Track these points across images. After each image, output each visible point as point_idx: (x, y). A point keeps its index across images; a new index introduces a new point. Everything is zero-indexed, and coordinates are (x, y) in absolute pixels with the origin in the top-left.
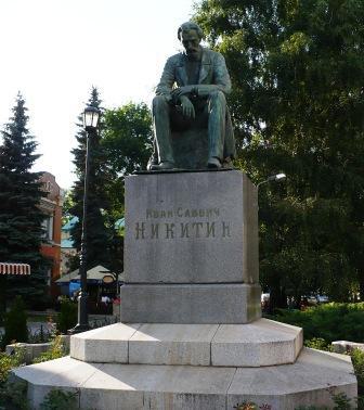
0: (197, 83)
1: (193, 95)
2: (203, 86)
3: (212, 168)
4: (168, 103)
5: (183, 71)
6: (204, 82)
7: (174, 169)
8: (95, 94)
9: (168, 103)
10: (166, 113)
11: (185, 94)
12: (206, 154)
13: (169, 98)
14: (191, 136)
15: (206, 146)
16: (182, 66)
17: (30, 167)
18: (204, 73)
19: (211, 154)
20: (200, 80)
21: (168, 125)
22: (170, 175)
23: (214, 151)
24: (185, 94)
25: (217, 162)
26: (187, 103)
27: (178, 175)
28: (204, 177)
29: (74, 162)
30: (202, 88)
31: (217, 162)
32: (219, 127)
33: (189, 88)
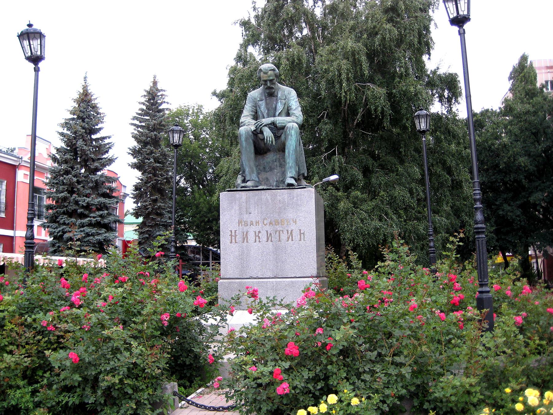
0: (274, 116)
1: (273, 127)
3: (290, 186)
4: (252, 132)
6: (280, 115)
9: (252, 132)
13: (253, 128)
14: (270, 157)
20: (277, 113)
24: (265, 125)
26: (268, 133)
28: (283, 194)
30: (280, 120)
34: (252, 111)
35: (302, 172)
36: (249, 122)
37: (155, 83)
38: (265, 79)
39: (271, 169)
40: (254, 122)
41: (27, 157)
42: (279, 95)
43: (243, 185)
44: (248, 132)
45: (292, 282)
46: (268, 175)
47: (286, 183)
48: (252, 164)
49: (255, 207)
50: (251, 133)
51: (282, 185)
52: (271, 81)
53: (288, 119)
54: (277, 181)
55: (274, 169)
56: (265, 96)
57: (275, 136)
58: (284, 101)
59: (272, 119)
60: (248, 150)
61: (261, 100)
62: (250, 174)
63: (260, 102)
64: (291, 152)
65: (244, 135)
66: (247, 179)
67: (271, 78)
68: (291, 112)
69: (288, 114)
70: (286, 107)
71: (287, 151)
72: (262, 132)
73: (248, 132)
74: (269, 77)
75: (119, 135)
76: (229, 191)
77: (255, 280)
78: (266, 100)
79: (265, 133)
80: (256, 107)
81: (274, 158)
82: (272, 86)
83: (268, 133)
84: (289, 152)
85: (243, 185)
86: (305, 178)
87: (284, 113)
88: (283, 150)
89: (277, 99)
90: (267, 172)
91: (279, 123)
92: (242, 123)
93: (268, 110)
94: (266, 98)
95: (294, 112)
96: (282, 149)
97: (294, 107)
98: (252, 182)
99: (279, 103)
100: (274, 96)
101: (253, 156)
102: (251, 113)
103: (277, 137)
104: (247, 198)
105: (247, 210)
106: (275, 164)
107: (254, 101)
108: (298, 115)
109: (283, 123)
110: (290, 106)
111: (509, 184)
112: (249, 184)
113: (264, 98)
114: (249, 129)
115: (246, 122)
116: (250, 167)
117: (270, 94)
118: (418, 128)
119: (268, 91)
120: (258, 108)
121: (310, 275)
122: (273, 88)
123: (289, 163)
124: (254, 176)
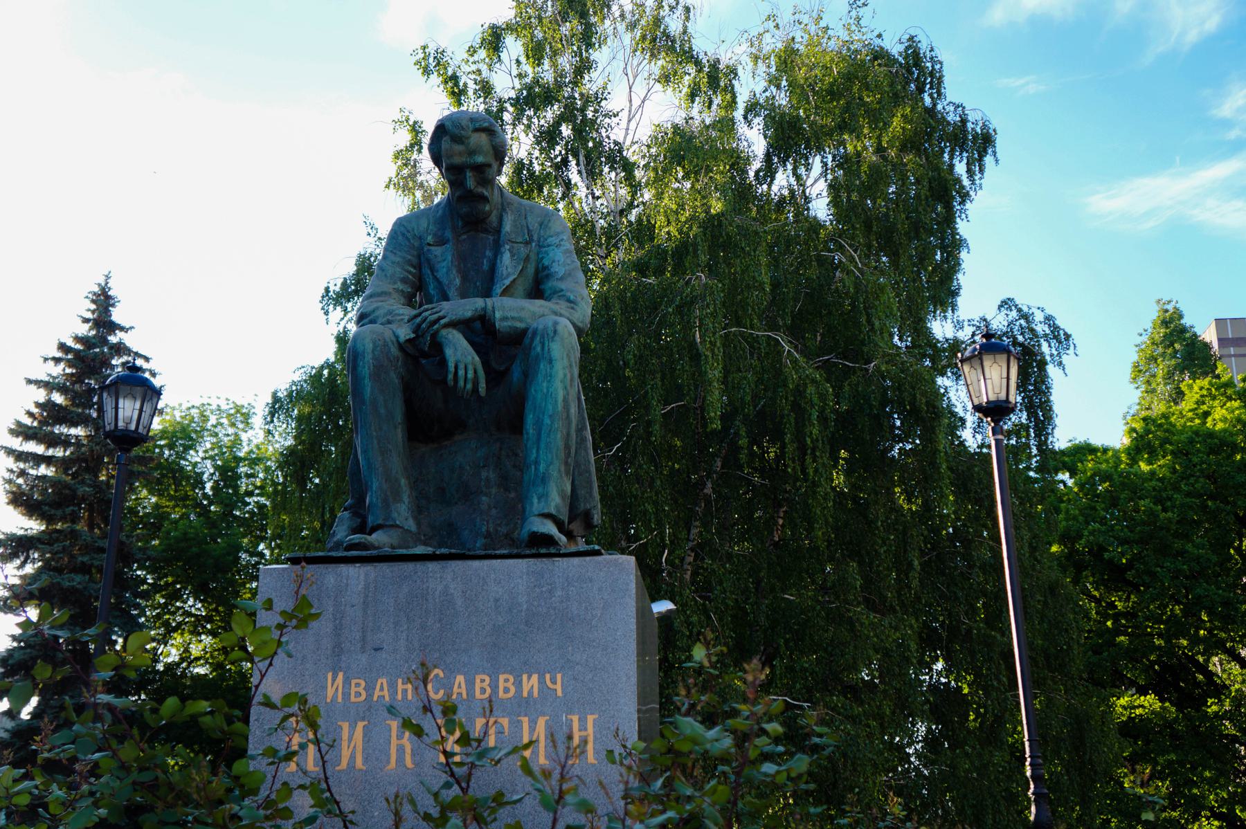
0: (487, 294)
1: (481, 331)
2: (508, 302)
3: (540, 546)
4: (401, 347)
5: (444, 259)
6: (506, 292)
7: (420, 550)
8: (104, 300)
9: (401, 347)
10: (394, 377)
11: (453, 324)
12: (515, 509)
13: (405, 333)
14: (467, 453)
15: (515, 483)
16: (441, 242)
17: (944, 293)
18: (508, 265)
19: (536, 506)
20: (498, 289)
21: (399, 416)
22: (409, 567)
23: (543, 497)
24: (453, 324)
25: (551, 528)
26: (460, 351)
27: (432, 566)
28: (511, 577)
29: (274, 395)
30: (510, 310)
31: (551, 528)
32: (558, 424)
33: (468, 307)
35: (582, 507)
36: (390, 312)
38: (457, 160)
40: (408, 312)
41: (322, 776)
42: (507, 227)
43: (357, 538)
44: (385, 345)
47: (525, 533)
48: (396, 463)
49: (396, 624)
50: (394, 351)
53: (537, 305)
58: (523, 251)
59: (479, 303)
60: (382, 411)
63: (437, 251)
65: (369, 357)
67: (480, 159)
68: (549, 285)
69: (537, 290)
70: (531, 270)
71: (530, 419)
72: (437, 348)
73: (385, 345)
75: (17, 444)
79: (449, 352)
82: (480, 190)
83: (460, 351)
85: (357, 538)
87: (520, 288)
88: (515, 424)
91: (504, 319)
97: (558, 269)
98: (393, 532)
100: (486, 231)
101: (399, 434)
102: (400, 286)
103: (495, 376)
104: (367, 587)
105: (364, 639)
106: (484, 474)
109: (520, 320)
110: (545, 268)
111: (1160, 636)
113: (449, 234)
114: (388, 334)
120: (426, 271)
121: (329, 774)
123: (537, 463)
124: (403, 513)
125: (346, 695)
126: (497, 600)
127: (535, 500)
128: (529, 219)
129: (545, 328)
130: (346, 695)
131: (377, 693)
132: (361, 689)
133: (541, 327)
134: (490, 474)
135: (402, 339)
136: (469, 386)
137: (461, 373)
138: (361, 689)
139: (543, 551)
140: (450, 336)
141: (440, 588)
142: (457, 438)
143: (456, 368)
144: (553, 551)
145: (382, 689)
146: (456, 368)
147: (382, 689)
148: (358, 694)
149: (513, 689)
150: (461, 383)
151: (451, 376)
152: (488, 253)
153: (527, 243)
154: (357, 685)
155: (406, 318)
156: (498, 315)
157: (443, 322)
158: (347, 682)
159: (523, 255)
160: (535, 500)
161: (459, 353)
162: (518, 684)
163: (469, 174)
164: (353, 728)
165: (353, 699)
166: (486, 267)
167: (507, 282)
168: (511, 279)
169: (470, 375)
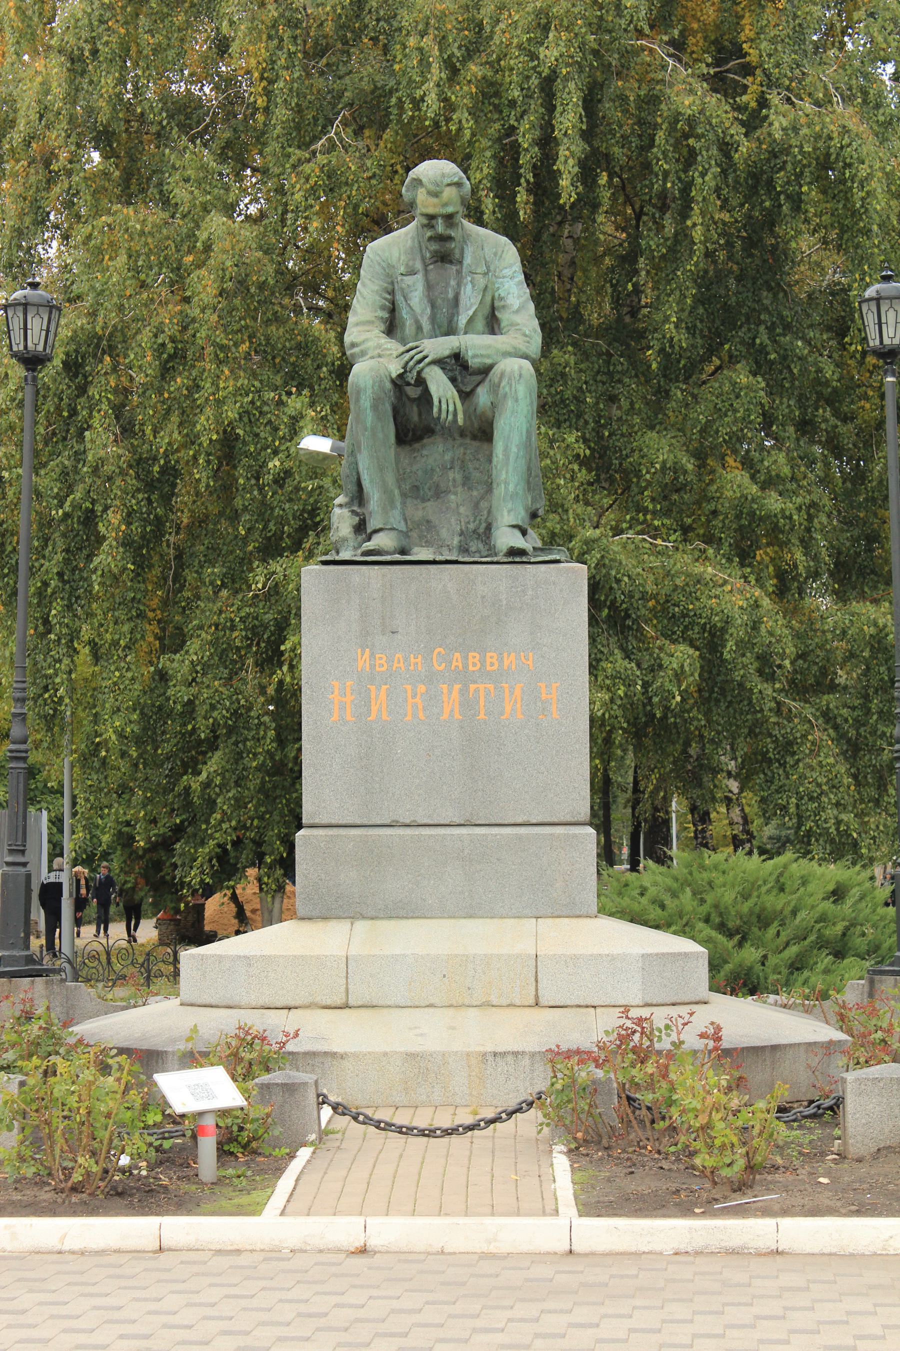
0: (450, 331)
1: (457, 365)
3: (516, 555)
4: (393, 381)
10: (388, 408)
13: (395, 369)
14: (436, 453)
20: (462, 320)
24: (434, 362)
26: (440, 386)
30: (476, 345)
34: (383, 308)
36: (379, 346)
37: (514, 526)
38: (431, 211)
39: (439, 493)
42: (468, 260)
45: (520, 837)
46: (430, 509)
50: (388, 385)
51: (477, 546)
52: (449, 218)
54: (462, 534)
55: (447, 492)
56: (423, 259)
57: (460, 391)
58: (481, 281)
60: (380, 435)
61: (412, 272)
62: (385, 511)
63: (409, 280)
64: (514, 449)
65: (369, 392)
66: (372, 525)
67: (450, 210)
68: (503, 316)
70: (488, 299)
74: (445, 205)
76: (325, 563)
77: (408, 831)
78: (426, 271)
80: (392, 293)
81: (448, 457)
83: (440, 386)
84: (506, 449)
86: (554, 537)
87: (480, 324)
89: (459, 272)
90: (424, 500)
92: (353, 345)
93: (433, 306)
94: (426, 266)
95: (518, 319)
96: (483, 432)
98: (393, 534)
99: (469, 286)
100: (451, 262)
106: (451, 475)
107: (388, 275)
108: (523, 323)
109: (488, 356)
110: (501, 299)
112: (381, 541)
113: (419, 265)
115: (370, 344)
116: (386, 491)
117: (442, 253)
118: (874, 342)
119: (434, 246)
120: (399, 298)
122: (450, 238)
123: (506, 483)
125: (373, 667)
126: (483, 597)
127: (505, 513)
128: (486, 249)
129: (512, 372)
130: (373, 667)
131: (396, 665)
132: (494, 660)
133: (508, 369)
134: (455, 475)
135: (394, 375)
136: (450, 417)
137: (444, 406)
138: (494, 660)
139: (518, 559)
140: (433, 374)
141: (440, 586)
142: (425, 441)
143: (440, 402)
144: (524, 559)
145: (399, 662)
146: (440, 402)
147: (399, 662)
148: (492, 664)
149: (496, 664)
150: (443, 415)
151: (435, 410)
152: (453, 283)
153: (486, 274)
154: (381, 658)
155: (395, 354)
156: (470, 354)
157: (427, 361)
158: (372, 655)
159: (482, 286)
160: (505, 513)
161: (441, 390)
162: (501, 661)
163: (440, 221)
164: (379, 688)
165: (471, 668)
166: (451, 295)
167: (471, 313)
168: (473, 309)
169: (451, 409)
